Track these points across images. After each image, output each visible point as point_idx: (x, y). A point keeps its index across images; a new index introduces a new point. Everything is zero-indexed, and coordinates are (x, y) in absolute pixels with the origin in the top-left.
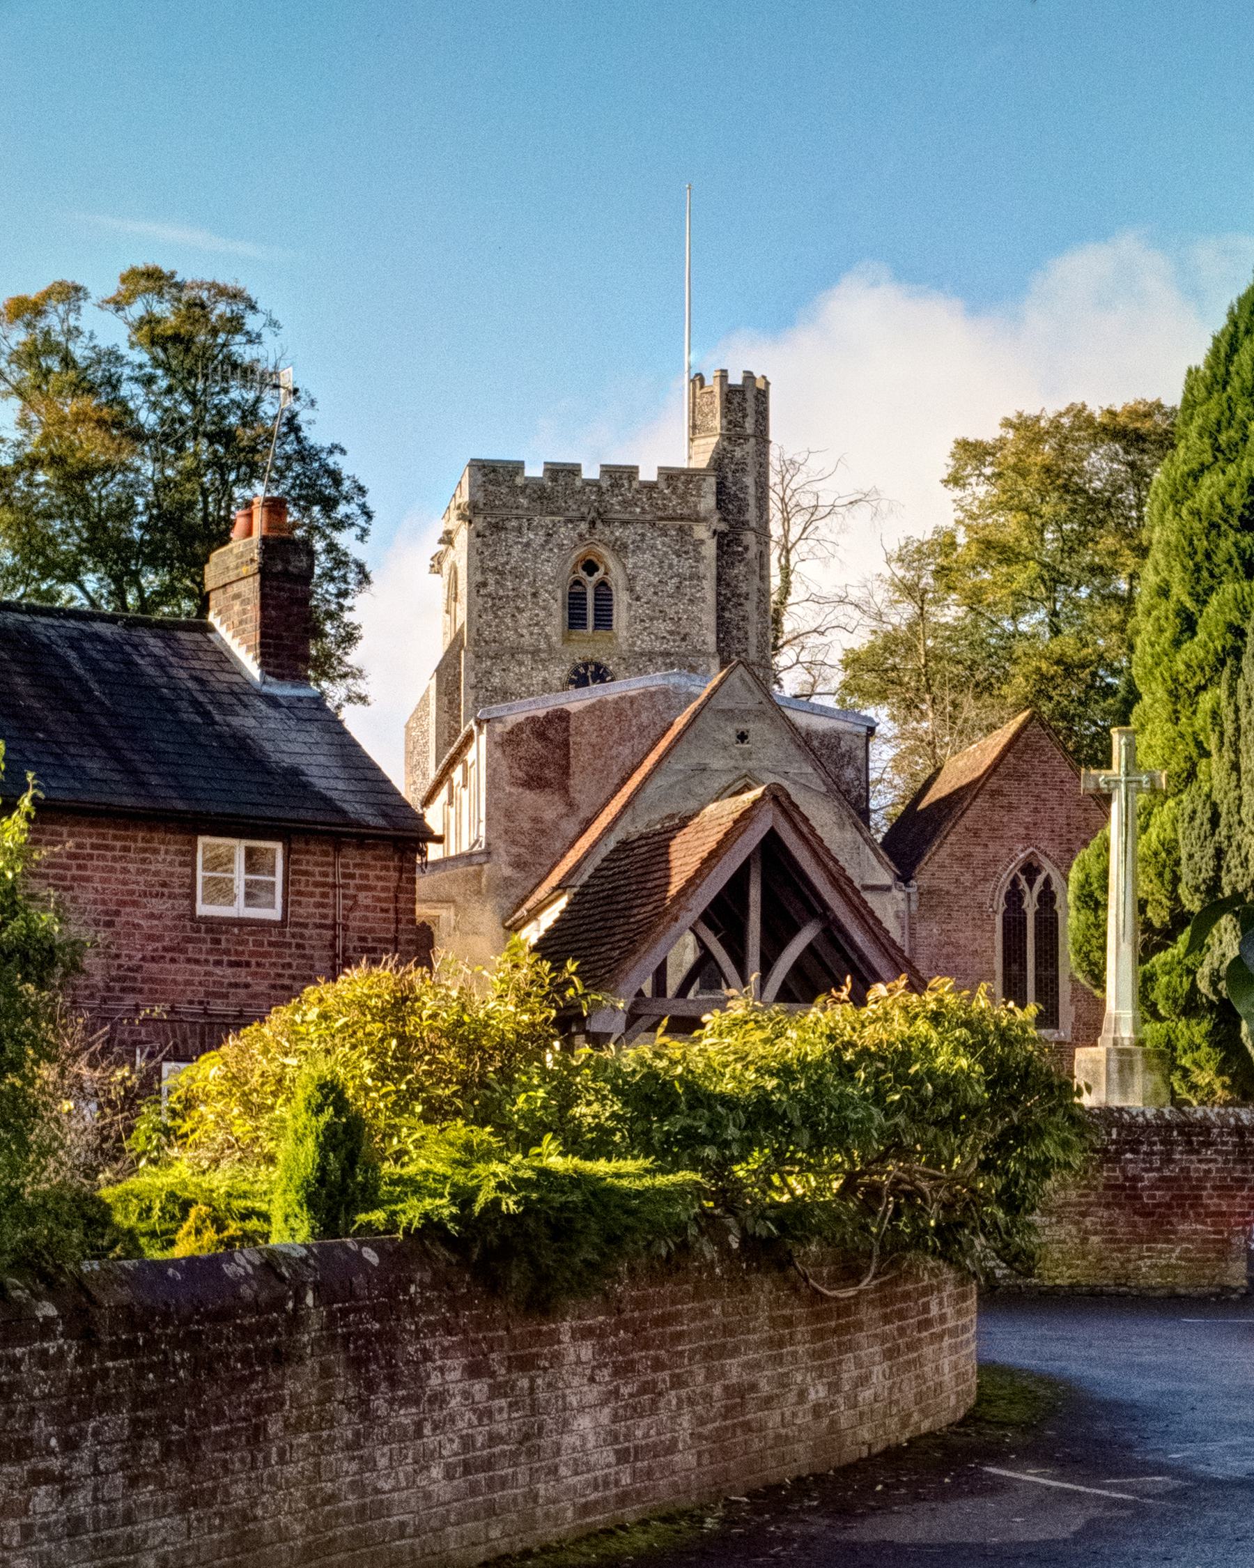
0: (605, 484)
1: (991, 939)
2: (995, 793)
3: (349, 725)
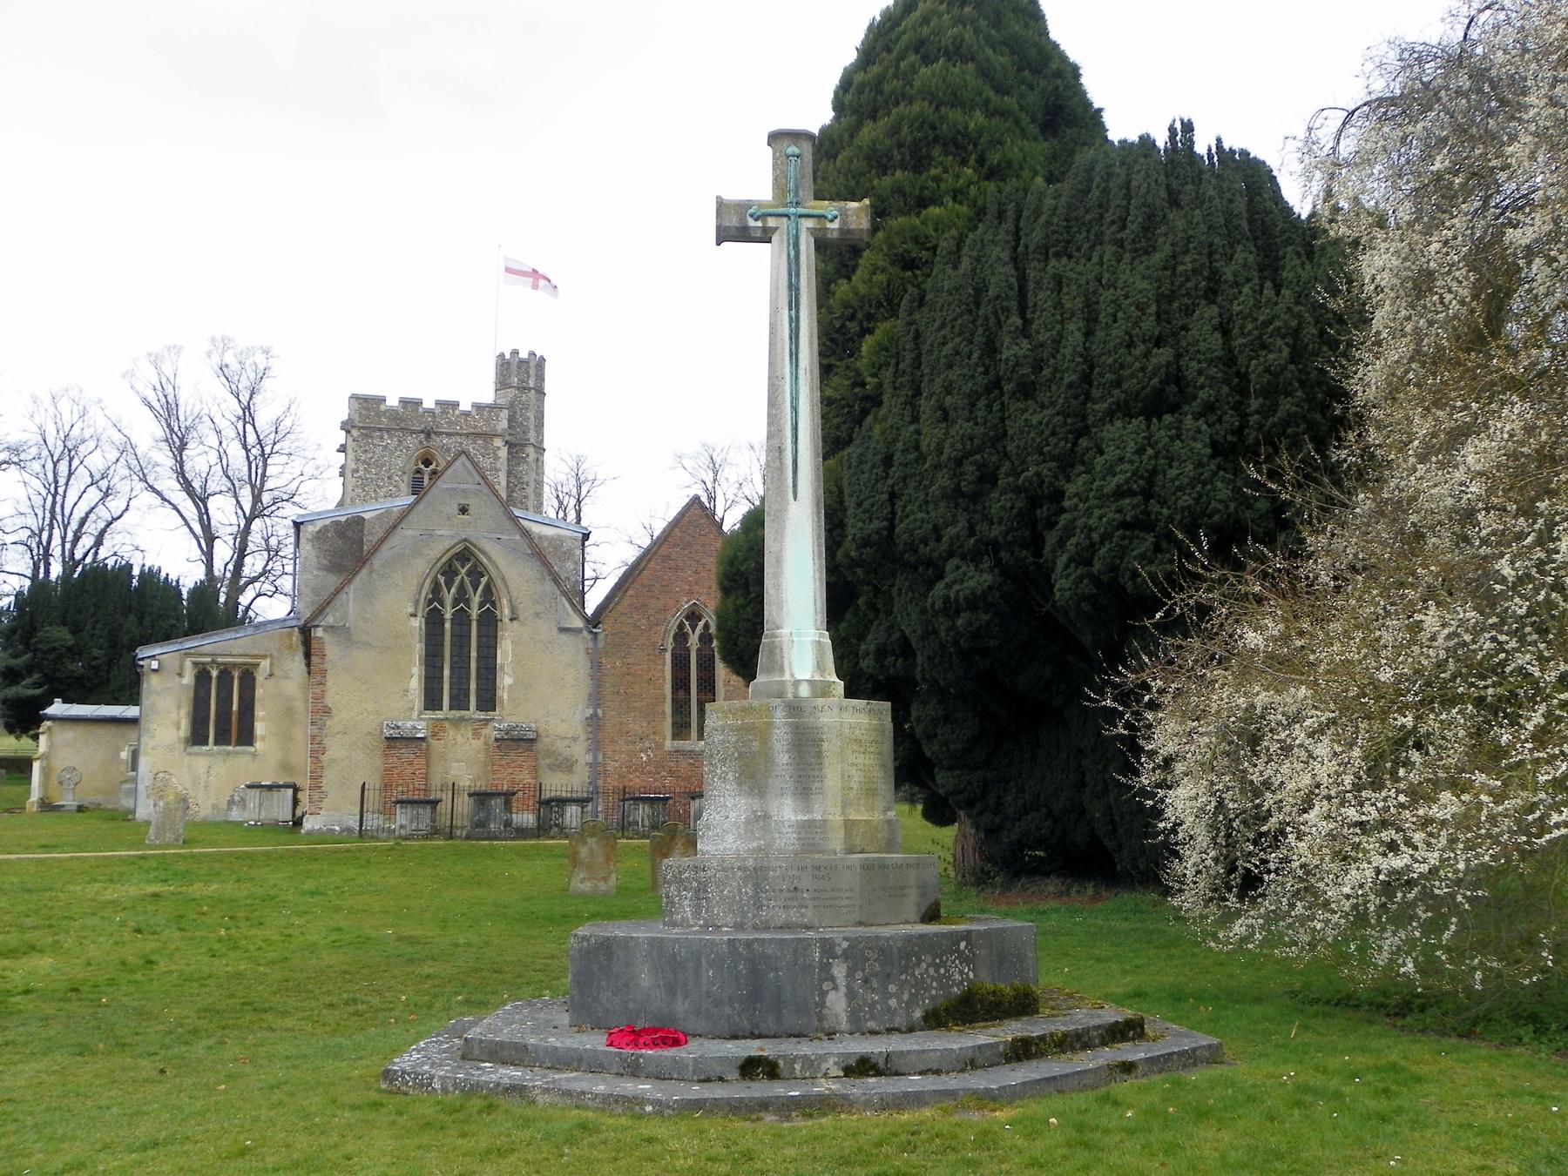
0: (438, 411)
1: (663, 671)
2: (668, 557)
3: (581, 711)
